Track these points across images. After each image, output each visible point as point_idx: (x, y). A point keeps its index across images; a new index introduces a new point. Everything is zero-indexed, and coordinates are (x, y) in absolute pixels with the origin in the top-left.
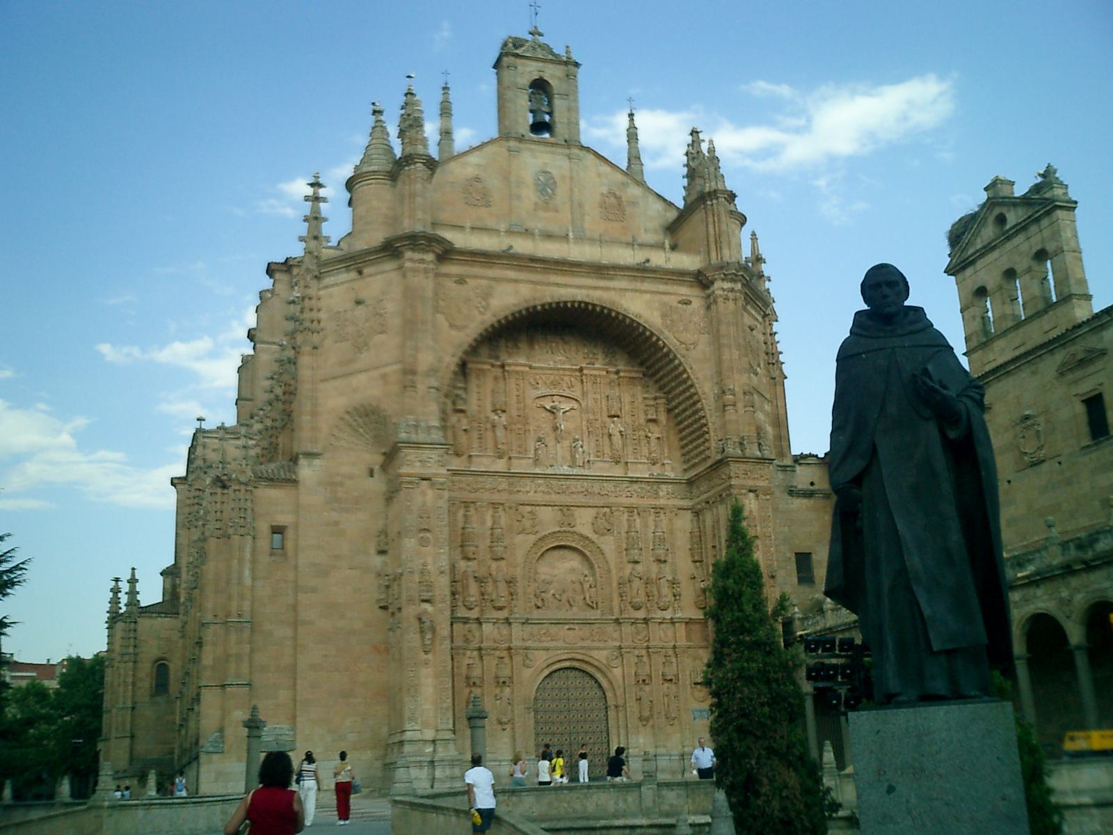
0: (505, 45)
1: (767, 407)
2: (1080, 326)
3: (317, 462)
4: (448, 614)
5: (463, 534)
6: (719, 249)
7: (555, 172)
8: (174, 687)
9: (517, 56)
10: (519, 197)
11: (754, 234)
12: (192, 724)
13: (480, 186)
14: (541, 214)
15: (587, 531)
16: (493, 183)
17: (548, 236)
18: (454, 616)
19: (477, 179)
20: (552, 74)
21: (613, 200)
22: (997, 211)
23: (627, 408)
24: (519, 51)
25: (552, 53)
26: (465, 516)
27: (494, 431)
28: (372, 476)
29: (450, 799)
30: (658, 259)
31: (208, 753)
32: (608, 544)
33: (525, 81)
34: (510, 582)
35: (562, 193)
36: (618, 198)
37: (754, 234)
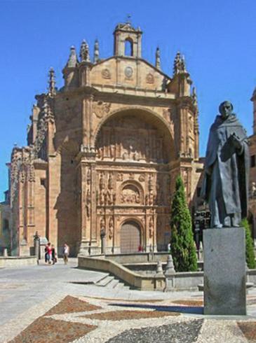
0: (117, 27)
1: (193, 142)
3: (54, 158)
4: (230, 229)
5: (101, 180)
6: (183, 92)
7: (133, 67)
8: (10, 226)
9: (121, 31)
10: (120, 76)
12: (17, 237)
14: (127, 81)
15: (137, 180)
16: (112, 71)
17: (130, 89)
18: (230, 225)
19: (106, 70)
20: (133, 36)
21: (150, 76)
23: (151, 141)
24: (122, 29)
27: (102, 239)
29: (93, 300)
30: (162, 96)
31: (22, 245)
32: (143, 184)
33: (123, 39)
34: (114, 196)
35: (134, 74)
36: (152, 76)
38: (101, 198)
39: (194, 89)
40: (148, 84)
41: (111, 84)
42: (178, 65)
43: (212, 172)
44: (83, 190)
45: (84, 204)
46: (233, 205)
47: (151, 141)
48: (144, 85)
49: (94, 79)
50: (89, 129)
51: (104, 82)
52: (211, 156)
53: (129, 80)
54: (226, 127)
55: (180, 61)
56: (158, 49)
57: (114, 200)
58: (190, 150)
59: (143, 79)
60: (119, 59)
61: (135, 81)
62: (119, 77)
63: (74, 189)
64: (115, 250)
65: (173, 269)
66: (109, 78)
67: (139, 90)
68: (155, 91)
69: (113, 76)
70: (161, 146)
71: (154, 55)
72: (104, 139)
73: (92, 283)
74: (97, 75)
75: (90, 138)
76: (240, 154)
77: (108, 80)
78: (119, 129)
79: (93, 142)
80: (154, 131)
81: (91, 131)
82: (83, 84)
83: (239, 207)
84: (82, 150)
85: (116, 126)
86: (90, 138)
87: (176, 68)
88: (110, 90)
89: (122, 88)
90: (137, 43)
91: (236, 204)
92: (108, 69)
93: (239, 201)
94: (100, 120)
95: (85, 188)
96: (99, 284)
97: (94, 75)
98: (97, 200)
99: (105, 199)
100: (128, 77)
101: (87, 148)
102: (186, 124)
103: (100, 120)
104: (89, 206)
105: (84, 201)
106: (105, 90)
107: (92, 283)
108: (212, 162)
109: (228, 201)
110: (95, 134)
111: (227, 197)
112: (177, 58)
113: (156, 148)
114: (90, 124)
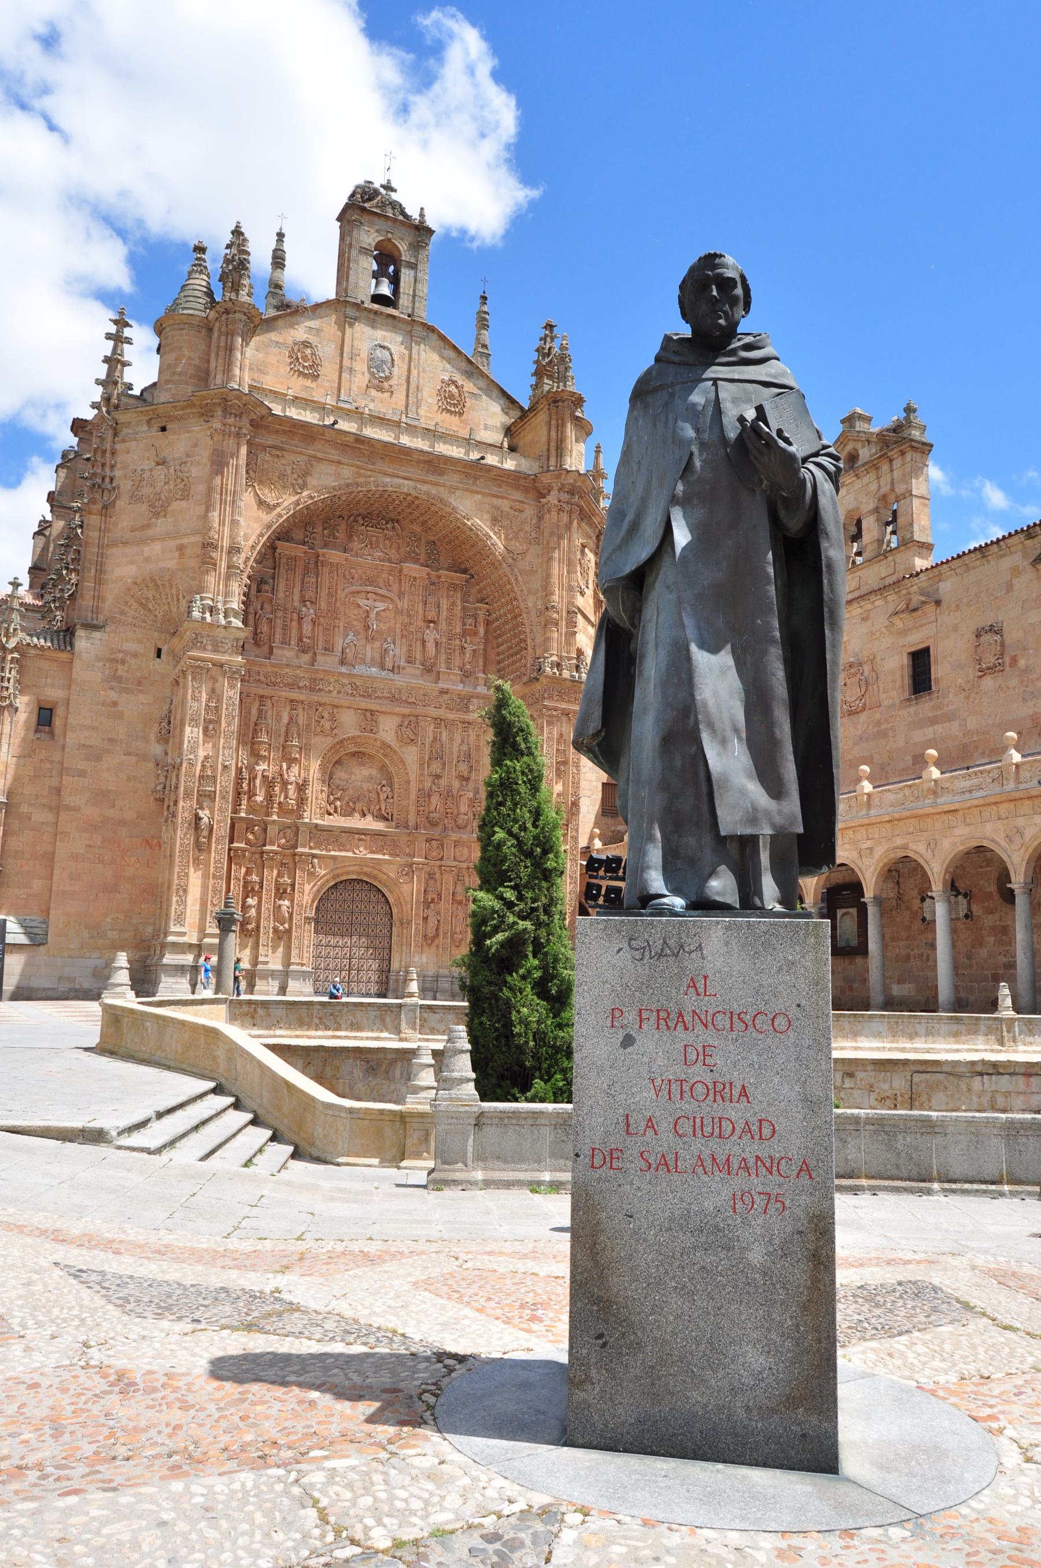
2: (918, 574)
3: (97, 635)
11: (598, 447)
13: (308, 351)
14: (373, 392)
16: (327, 350)
17: (381, 421)
18: (733, 898)
21: (453, 388)
22: (849, 447)
25: (403, 212)
26: (260, 711)
28: (159, 656)
34: (301, 788)
35: (399, 372)
37: (598, 447)
38: (251, 794)
39: (598, 450)
40: (446, 416)
41: (318, 397)
42: (550, 365)
43: (636, 612)
44: (187, 756)
45: (184, 808)
46: (755, 790)
47: (444, 614)
48: (429, 413)
49: (260, 368)
50: (226, 543)
51: (296, 386)
52: (634, 528)
53: (380, 389)
54: (715, 381)
55: (556, 350)
56: (484, 298)
57: (302, 801)
58: (580, 652)
59: (430, 398)
60: (350, 311)
61: (400, 397)
62: (345, 375)
63: (157, 749)
64: (293, 985)
65: (470, 1089)
66: (315, 377)
67: (412, 430)
68: (469, 442)
69: (328, 370)
70: (481, 630)
71: (474, 321)
72: (282, 587)
73: (95, 1136)
74: (273, 359)
75: (228, 577)
76: (794, 523)
77: (308, 383)
78: (334, 556)
79: (237, 589)
80: (459, 578)
81: (234, 550)
82: (219, 379)
83: (793, 804)
84: (196, 614)
85: (326, 545)
86: (228, 577)
87: (540, 373)
88: (309, 417)
89: (356, 414)
90: (413, 266)
91: (775, 789)
92: (312, 339)
93: (790, 770)
94: (266, 518)
95: (193, 750)
96: (136, 1139)
97: (261, 355)
98: (238, 794)
99: (269, 797)
100: (379, 383)
101: (212, 610)
102: (570, 563)
103: (266, 518)
104: (204, 814)
105: (188, 795)
106: (293, 413)
107: (95, 1136)
108: (641, 553)
109: (728, 760)
110: (246, 559)
111: (724, 742)
112: (544, 339)
113: (464, 634)
114: (234, 523)
